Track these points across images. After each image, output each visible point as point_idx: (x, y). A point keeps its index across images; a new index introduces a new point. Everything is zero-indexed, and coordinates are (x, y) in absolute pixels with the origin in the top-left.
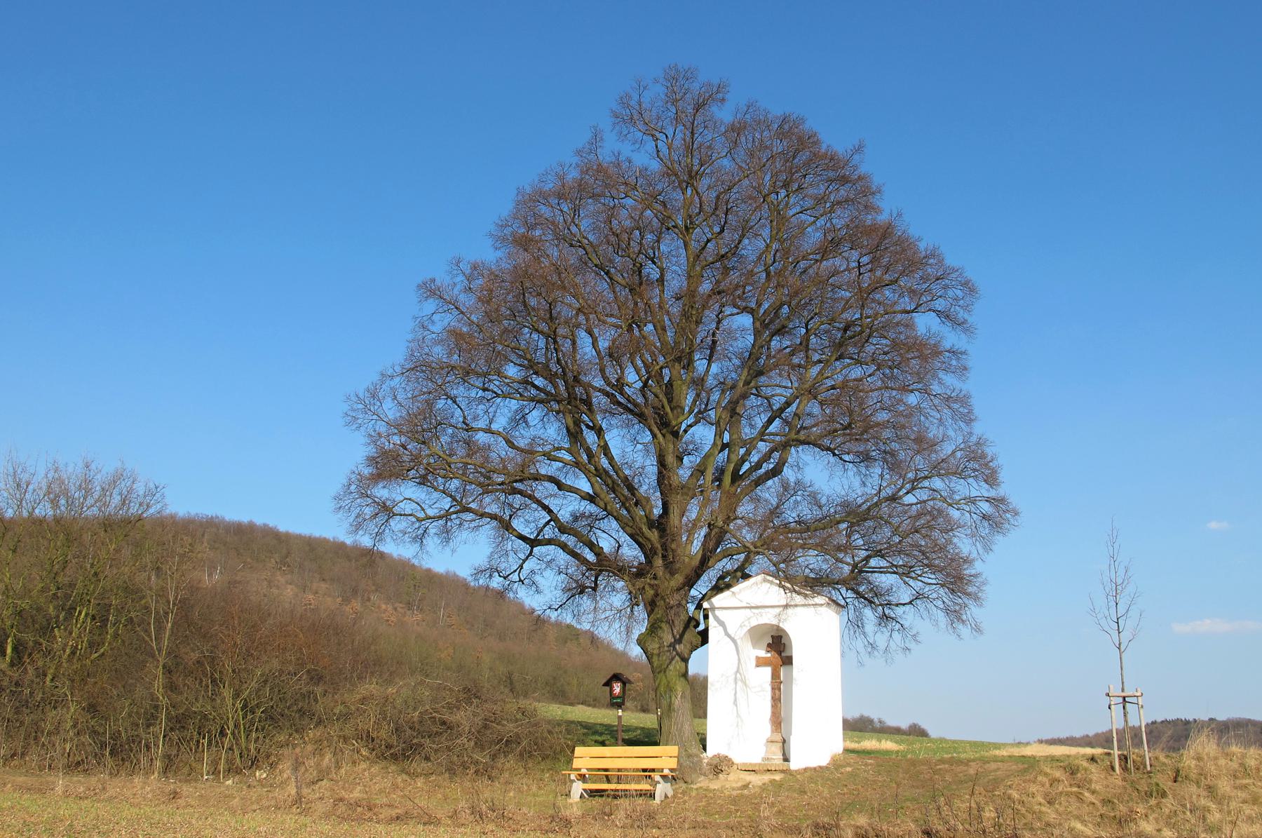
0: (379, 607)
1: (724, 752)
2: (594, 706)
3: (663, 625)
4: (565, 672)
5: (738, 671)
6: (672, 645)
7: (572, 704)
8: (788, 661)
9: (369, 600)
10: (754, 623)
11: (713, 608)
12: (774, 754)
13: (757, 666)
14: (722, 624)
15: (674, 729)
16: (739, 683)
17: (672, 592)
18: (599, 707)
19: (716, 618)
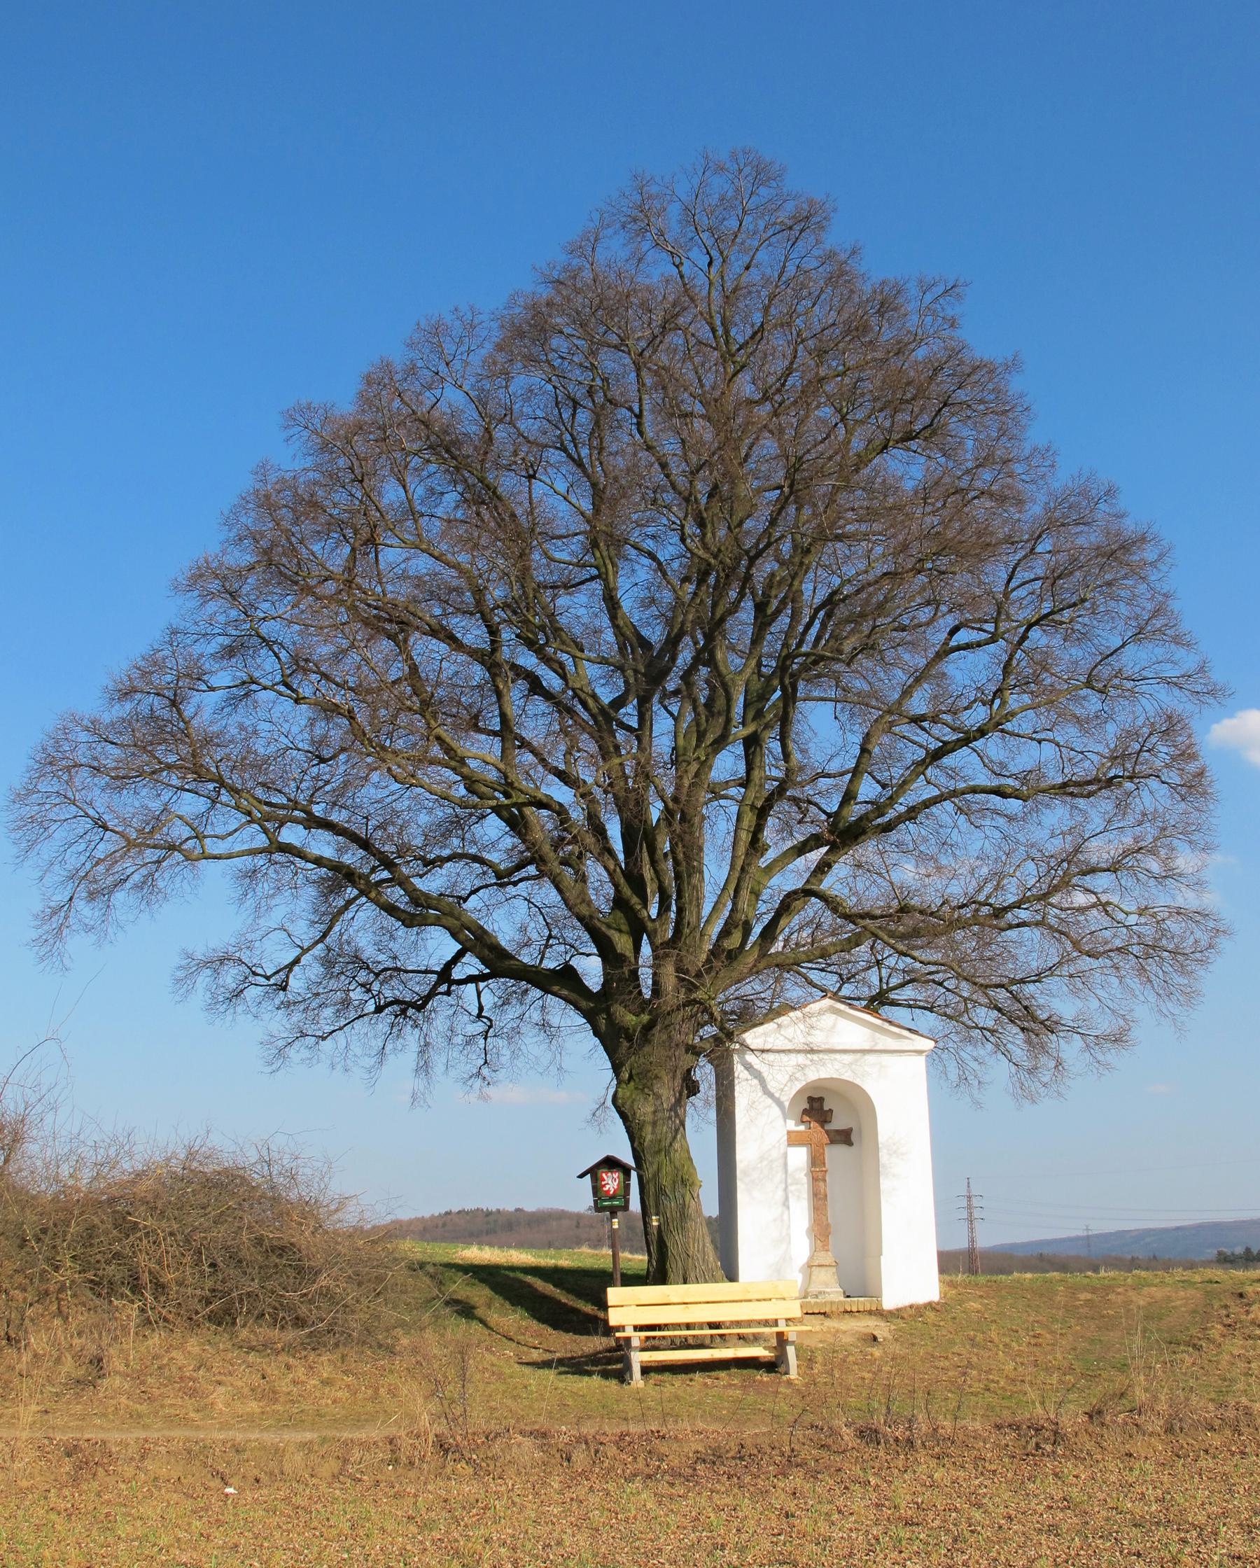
12: (827, 1285)
14: (757, 1075)
19: (748, 1067)
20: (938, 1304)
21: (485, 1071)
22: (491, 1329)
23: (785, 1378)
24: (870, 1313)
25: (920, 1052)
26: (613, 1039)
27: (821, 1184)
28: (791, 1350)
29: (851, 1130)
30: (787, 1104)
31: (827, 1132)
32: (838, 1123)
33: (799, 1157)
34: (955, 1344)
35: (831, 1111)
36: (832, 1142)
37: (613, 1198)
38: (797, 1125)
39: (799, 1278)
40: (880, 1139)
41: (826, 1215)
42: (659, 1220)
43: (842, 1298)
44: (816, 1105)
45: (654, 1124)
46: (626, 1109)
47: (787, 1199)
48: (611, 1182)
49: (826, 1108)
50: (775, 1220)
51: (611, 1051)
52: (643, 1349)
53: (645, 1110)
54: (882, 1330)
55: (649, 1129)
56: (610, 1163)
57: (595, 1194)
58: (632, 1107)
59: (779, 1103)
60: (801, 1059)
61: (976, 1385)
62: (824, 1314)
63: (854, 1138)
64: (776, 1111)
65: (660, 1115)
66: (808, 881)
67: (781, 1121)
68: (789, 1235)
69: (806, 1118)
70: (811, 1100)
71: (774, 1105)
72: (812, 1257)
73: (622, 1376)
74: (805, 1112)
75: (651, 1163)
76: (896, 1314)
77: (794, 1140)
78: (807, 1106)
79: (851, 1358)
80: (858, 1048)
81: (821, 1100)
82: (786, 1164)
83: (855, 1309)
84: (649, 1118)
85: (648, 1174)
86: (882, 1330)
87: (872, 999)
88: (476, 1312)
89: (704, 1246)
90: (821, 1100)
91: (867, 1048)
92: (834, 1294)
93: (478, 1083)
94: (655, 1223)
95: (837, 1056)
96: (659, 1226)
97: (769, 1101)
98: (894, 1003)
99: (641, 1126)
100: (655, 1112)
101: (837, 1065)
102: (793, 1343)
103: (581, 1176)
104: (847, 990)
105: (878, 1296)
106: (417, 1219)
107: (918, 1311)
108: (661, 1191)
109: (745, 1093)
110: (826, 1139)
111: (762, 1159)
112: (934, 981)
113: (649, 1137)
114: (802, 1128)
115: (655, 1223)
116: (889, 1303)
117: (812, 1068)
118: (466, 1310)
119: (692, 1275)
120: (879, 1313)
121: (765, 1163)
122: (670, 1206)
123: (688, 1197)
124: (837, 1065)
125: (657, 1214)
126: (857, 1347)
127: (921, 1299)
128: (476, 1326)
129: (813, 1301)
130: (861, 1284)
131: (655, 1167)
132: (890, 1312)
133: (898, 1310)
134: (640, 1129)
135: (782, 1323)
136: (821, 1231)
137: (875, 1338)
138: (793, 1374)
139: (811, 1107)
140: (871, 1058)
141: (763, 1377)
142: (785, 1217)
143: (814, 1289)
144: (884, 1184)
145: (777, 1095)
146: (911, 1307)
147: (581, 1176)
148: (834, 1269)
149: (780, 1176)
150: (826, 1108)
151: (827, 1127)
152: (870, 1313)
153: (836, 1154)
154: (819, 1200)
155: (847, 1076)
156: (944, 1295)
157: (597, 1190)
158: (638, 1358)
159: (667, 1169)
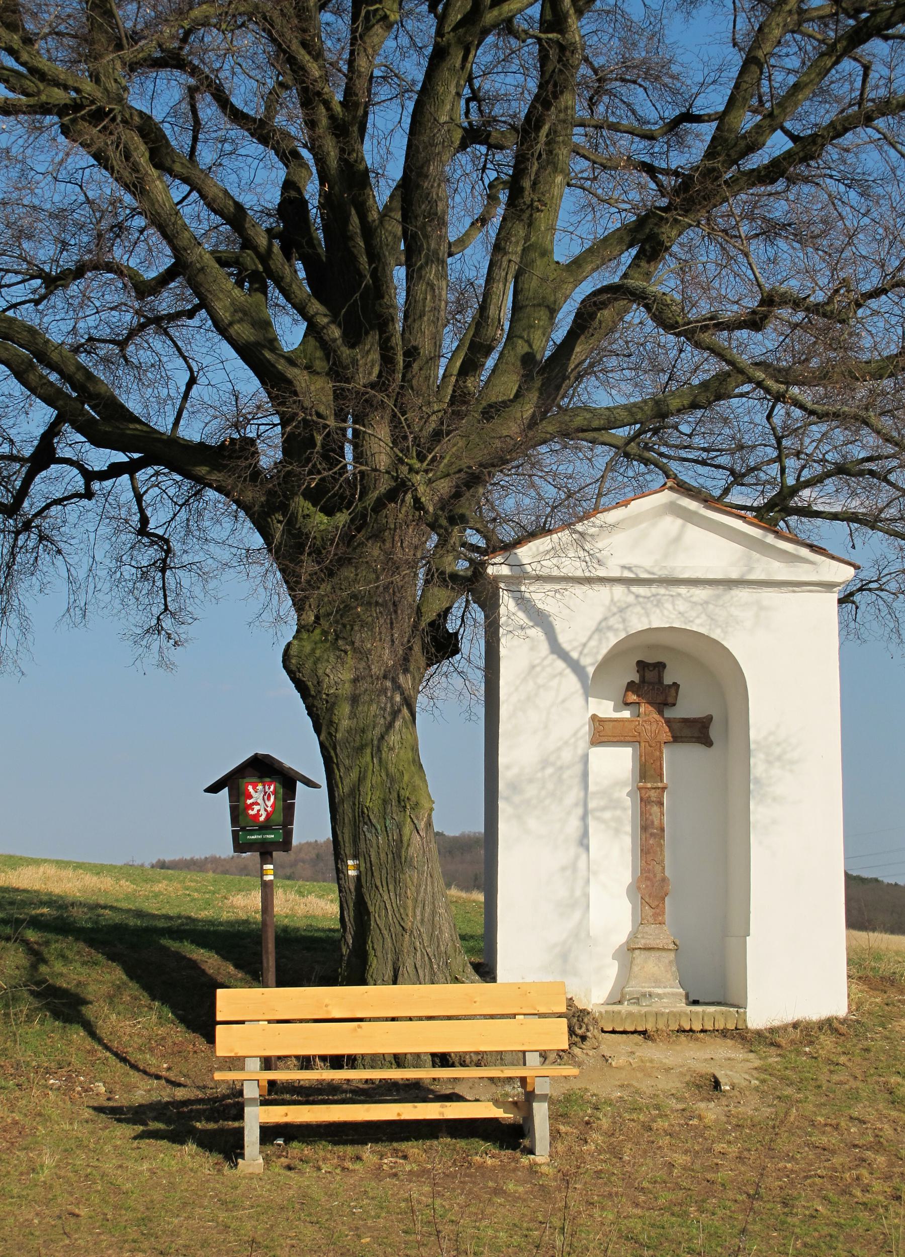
10: (638, 623)
12: (657, 982)
14: (541, 619)
19: (523, 602)
20: (843, 1021)
21: (167, 623)
22: (100, 1041)
23: (525, 1160)
24: (724, 1033)
25: (828, 586)
26: (289, 552)
27: (655, 809)
28: (541, 1112)
29: (710, 718)
30: (591, 670)
31: (668, 722)
32: (688, 707)
33: (616, 764)
34: (857, 1099)
35: (676, 686)
36: (676, 739)
37: (265, 827)
38: (616, 710)
39: (612, 970)
40: (754, 734)
41: (661, 863)
42: (358, 867)
43: (682, 1006)
44: (650, 675)
45: (355, 700)
46: (305, 676)
47: (585, 834)
48: (261, 799)
49: (668, 680)
50: (564, 869)
51: (291, 580)
52: (265, 1103)
53: (338, 676)
54: (733, 1065)
55: (345, 709)
56: (262, 767)
57: (235, 820)
58: (314, 671)
59: (576, 667)
60: (619, 591)
61: (877, 1186)
62: (644, 1033)
63: (714, 732)
64: (572, 682)
65: (364, 685)
66: (625, 276)
67: (579, 699)
68: (587, 896)
69: (633, 698)
70: (642, 666)
71: (568, 671)
72: (634, 935)
73: (230, 1147)
74: (631, 687)
75: (348, 769)
76: (768, 1039)
77: (603, 733)
78: (636, 678)
79: (660, 1124)
80: (719, 576)
81: (660, 666)
82: (585, 775)
83: (697, 1027)
84: (346, 689)
85: (344, 788)
86: (733, 1065)
87: (770, 505)
88: (84, 1009)
89: (434, 913)
90: (660, 666)
91: (734, 575)
92: (668, 998)
93: (157, 642)
94: (352, 873)
95: (683, 590)
96: (358, 877)
97: (560, 665)
98: (808, 512)
99: (331, 707)
100: (355, 681)
101: (681, 606)
102: (544, 1098)
103: (214, 789)
104: (737, 497)
105: (740, 1005)
106: (308, 844)
107: (807, 1032)
108: (361, 817)
109: (518, 652)
110: (665, 734)
111: (545, 763)
112: (872, 473)
113: (345, 723)
114: (626, 714)
115: (352, 873)
116: (758, 1017)
118: (66, 1007)
119: (409, 963)
120: (741, 1035)
121: (550, 771)
122: (377, 842)
123: (407, 829)
124: (681, 606)
125: (355, 857)
126: (679, 1099)
127: (815, 1013)
128: (78, 1035)
129: (634, 1009)
130: (714, 983)
131: (354, 775)
132: (759, 1033)
133: (772, 1030)
134: (330, 710)
135: (533, 1059)
136: (652, 890)
137: (717, 1085)
138: (542, 1155)
139: (643, 680)
140: (742, 594)
141: (487, 1156)
142: (582, 864)
143: (634, 988)
144: (758, 812)
145: (575, 655)
146: (795, 1025)
147: (214, 789)
148: (672, 955)
149: (574, 794)
150: (668, 680)
151: (669, 713)
152: (724, 1033)
153: (678, 761)
154: (650, 836)
155: (699, 626)
156: (856, 1005)
157: (238, 813)
158: (255, 1117)
159: (374, 779)
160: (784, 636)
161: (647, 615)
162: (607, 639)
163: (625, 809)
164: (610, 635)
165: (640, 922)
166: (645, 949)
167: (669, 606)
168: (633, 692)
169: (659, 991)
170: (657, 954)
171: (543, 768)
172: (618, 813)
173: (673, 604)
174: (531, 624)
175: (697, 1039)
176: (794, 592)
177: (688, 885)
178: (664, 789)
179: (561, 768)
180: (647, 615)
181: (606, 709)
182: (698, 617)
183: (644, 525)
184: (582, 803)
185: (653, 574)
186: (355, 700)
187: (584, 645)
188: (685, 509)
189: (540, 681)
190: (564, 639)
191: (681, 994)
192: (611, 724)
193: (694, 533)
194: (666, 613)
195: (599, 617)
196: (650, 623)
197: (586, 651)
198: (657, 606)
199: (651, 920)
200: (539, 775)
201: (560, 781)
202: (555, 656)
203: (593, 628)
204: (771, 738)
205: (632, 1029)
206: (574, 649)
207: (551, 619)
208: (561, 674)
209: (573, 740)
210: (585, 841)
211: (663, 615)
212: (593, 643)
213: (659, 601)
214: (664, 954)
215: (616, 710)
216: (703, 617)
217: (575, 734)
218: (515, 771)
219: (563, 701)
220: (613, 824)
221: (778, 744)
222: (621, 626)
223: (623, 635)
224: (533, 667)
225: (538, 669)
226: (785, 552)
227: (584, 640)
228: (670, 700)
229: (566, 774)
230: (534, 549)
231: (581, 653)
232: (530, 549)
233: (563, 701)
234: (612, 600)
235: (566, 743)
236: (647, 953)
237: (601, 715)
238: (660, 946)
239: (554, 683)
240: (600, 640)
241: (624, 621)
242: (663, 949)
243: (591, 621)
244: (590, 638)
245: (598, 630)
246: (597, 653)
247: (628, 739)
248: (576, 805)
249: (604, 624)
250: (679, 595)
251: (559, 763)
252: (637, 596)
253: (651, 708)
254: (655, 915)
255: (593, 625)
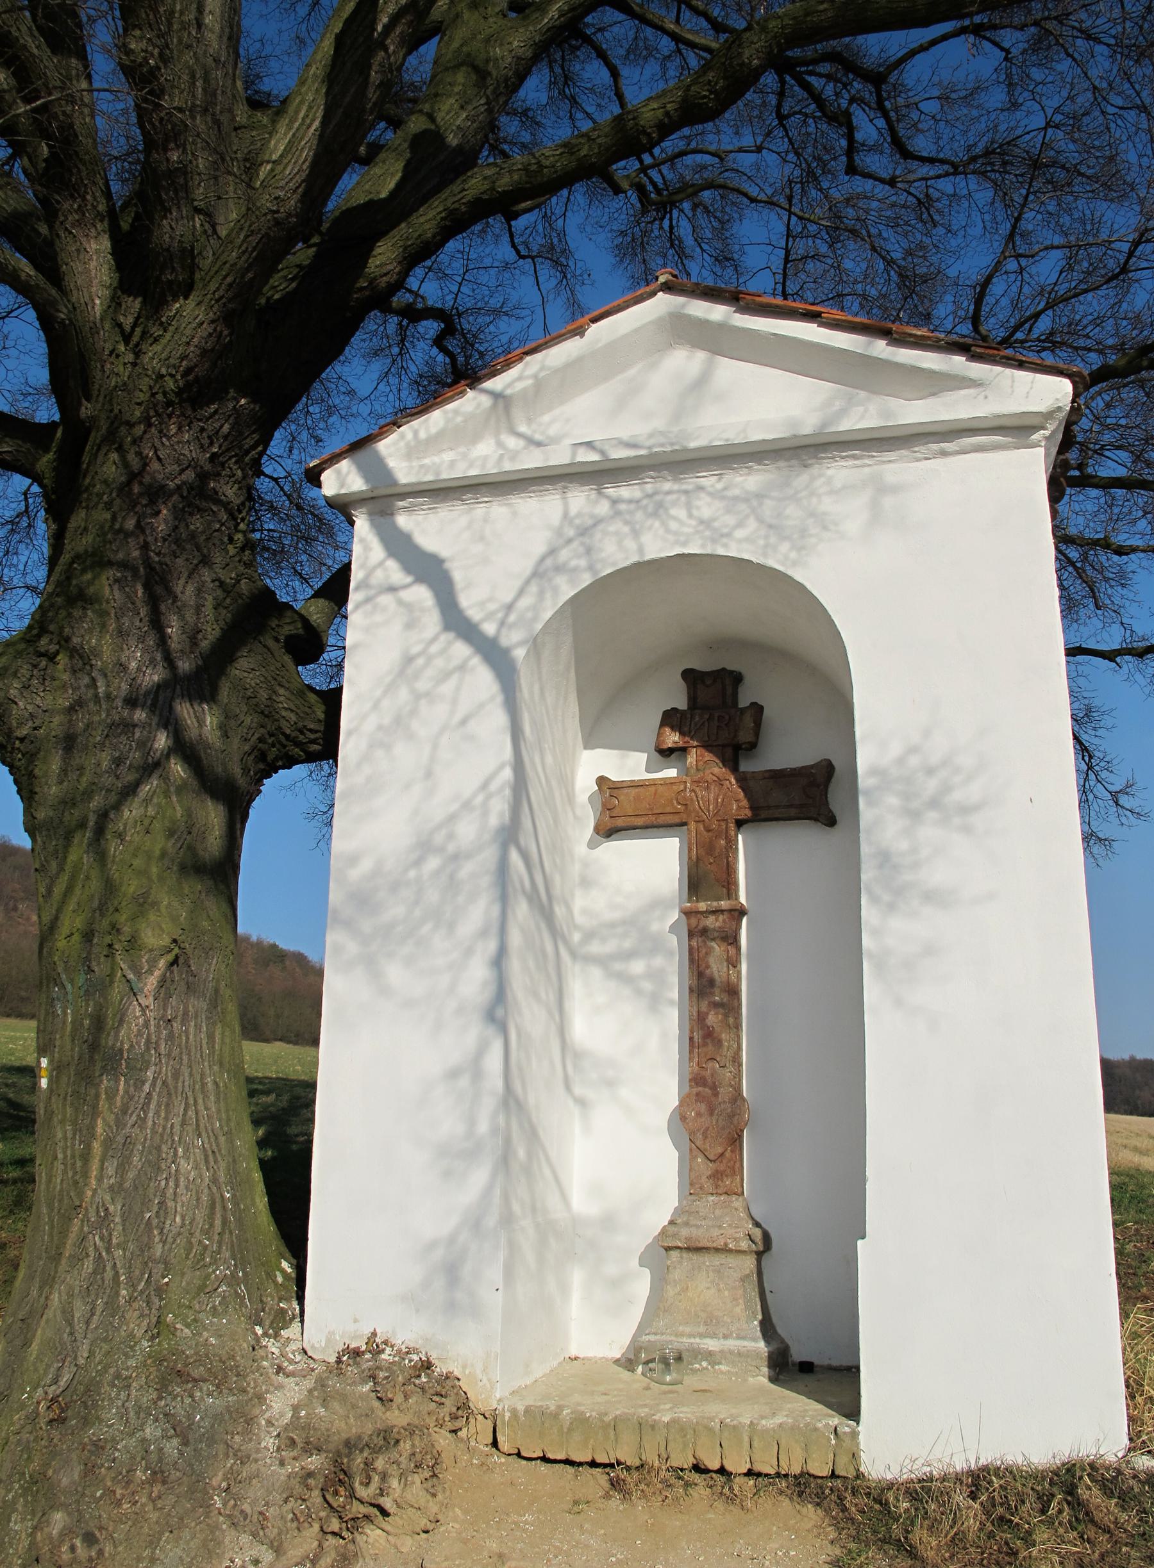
0: (28, 919)
1: (407, 1331)
2: (296, 1043)
3: (105, 586)
4: (260, 999)
5: (509, 835)
6: (160, 703)
7: (267, 1041)
8: (812, 796)
9: (15, 909)
10: (617, 552)
11: (384, 499)
12: (712, 1324)
13: (608, 830)
14: (429, 570)
15: (98, 1188)
16: (522, 910)
17: (161, 409)
18: (302, 1044)
19: (401, 547)
25: (1016, 429)
27: (718, 949)
32: (787, 749)
45: (69, 742)
49: (744, 702)
50: (453, 1074)
60: (579, 499)
63: (836, 800)
69: (672, 738)
74: (670, 719)
97: (461, 650)
110: (739, 805)
111: (424, 847)
117: (617, 526)
121: (433, 863)
124: (706, 507)
136: (714, 1123)
140: (839, 471)
145: (490, 629)
150: (744, 702)
154: (711, 1001)
155: (742, 544)
160: (925, 541)
161: (636, 534)
162: (556, 590)
163: (671, 953)
164: (561, 581)
165: (691, 1187)
166: (688, 1249)
167: (680, 512)
168: (673, 729)
169: (712, 1344)
170: (717, 1260)
171: (418, 862)
172: (658, 961)
173: (689, 507)
174: (409, 579)
175: (731, 1499)
176: (944, 454)
177: (763, 1106)
178: (742, 912)
179: (456, 858)
180: (636, 534)
181: (631, 766)
182: (740, 525)
183: (632, 372)
184: (495, 930)
185: (635, 446)
186: (69, 742)
187: (509, 607)
188: (704, 324)
189: (422, 685)
190: (469, 602)
191: (758, 1355)
192: (633, 791)
193: (729, 370)
194: (673, 525)
195: (540, 549)
196: (641, 550)
197: (512, 618)
198: (655, 514)
199: (708, 1186)
200: (412, 874)
201: (452, 885)
202: (451, 635)
203: (528, 572)
204: (914, 761)
205: (561, 1456)
206: (489, 617)
207: (447, 565)
208: (462, 668)
209: (480, 798)
210: (500, 1012)
211: (668, 531)
212: (526, 602)
213: (660, 505)
214: (731, 1260)
215: (648, 770)
216: (752, 524)
217: (485, 786)
218: (367, 865)
219: (464, 722)
220: (647, 986)
221: (930, 771)
222: (583, 563)
223: (586, 580)
224: (409, 660)
225: (420, 661)
226: (931, 373)
227: (508, 598)
228: (744, 737)
229: (467, 869)
230: (409, 436)
231: (502, 623)
232: (403, 437)
233: (464, 722)
234: (566, 515)
235: (467, 805)
236: (696, 1258)
237: (614, 777)
238: (720, 1243)
239: (447, 688)
240: (541, 594)
241: (589, 551)
242: (725, 1250)
243: (504, 556)
244: (521, 592)
245: (537, 574)
246: (535, 619)
247: (662, 819)
248: (483, 933)
249: (549, 562)
250: (701, 488)
251: (451, 848)
252: (615, 502)
253: (708, 756)
254: (717, 1176)
255: (526, 566)
